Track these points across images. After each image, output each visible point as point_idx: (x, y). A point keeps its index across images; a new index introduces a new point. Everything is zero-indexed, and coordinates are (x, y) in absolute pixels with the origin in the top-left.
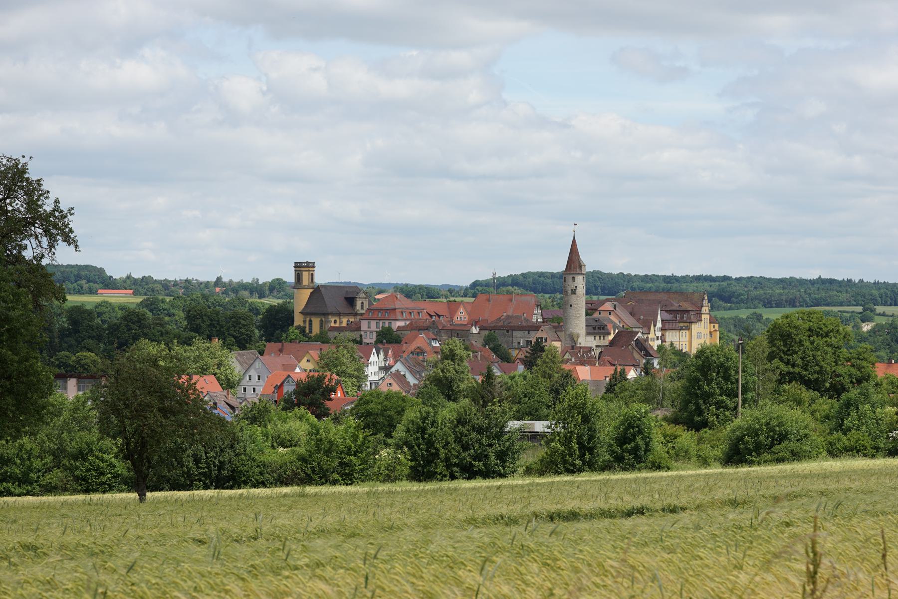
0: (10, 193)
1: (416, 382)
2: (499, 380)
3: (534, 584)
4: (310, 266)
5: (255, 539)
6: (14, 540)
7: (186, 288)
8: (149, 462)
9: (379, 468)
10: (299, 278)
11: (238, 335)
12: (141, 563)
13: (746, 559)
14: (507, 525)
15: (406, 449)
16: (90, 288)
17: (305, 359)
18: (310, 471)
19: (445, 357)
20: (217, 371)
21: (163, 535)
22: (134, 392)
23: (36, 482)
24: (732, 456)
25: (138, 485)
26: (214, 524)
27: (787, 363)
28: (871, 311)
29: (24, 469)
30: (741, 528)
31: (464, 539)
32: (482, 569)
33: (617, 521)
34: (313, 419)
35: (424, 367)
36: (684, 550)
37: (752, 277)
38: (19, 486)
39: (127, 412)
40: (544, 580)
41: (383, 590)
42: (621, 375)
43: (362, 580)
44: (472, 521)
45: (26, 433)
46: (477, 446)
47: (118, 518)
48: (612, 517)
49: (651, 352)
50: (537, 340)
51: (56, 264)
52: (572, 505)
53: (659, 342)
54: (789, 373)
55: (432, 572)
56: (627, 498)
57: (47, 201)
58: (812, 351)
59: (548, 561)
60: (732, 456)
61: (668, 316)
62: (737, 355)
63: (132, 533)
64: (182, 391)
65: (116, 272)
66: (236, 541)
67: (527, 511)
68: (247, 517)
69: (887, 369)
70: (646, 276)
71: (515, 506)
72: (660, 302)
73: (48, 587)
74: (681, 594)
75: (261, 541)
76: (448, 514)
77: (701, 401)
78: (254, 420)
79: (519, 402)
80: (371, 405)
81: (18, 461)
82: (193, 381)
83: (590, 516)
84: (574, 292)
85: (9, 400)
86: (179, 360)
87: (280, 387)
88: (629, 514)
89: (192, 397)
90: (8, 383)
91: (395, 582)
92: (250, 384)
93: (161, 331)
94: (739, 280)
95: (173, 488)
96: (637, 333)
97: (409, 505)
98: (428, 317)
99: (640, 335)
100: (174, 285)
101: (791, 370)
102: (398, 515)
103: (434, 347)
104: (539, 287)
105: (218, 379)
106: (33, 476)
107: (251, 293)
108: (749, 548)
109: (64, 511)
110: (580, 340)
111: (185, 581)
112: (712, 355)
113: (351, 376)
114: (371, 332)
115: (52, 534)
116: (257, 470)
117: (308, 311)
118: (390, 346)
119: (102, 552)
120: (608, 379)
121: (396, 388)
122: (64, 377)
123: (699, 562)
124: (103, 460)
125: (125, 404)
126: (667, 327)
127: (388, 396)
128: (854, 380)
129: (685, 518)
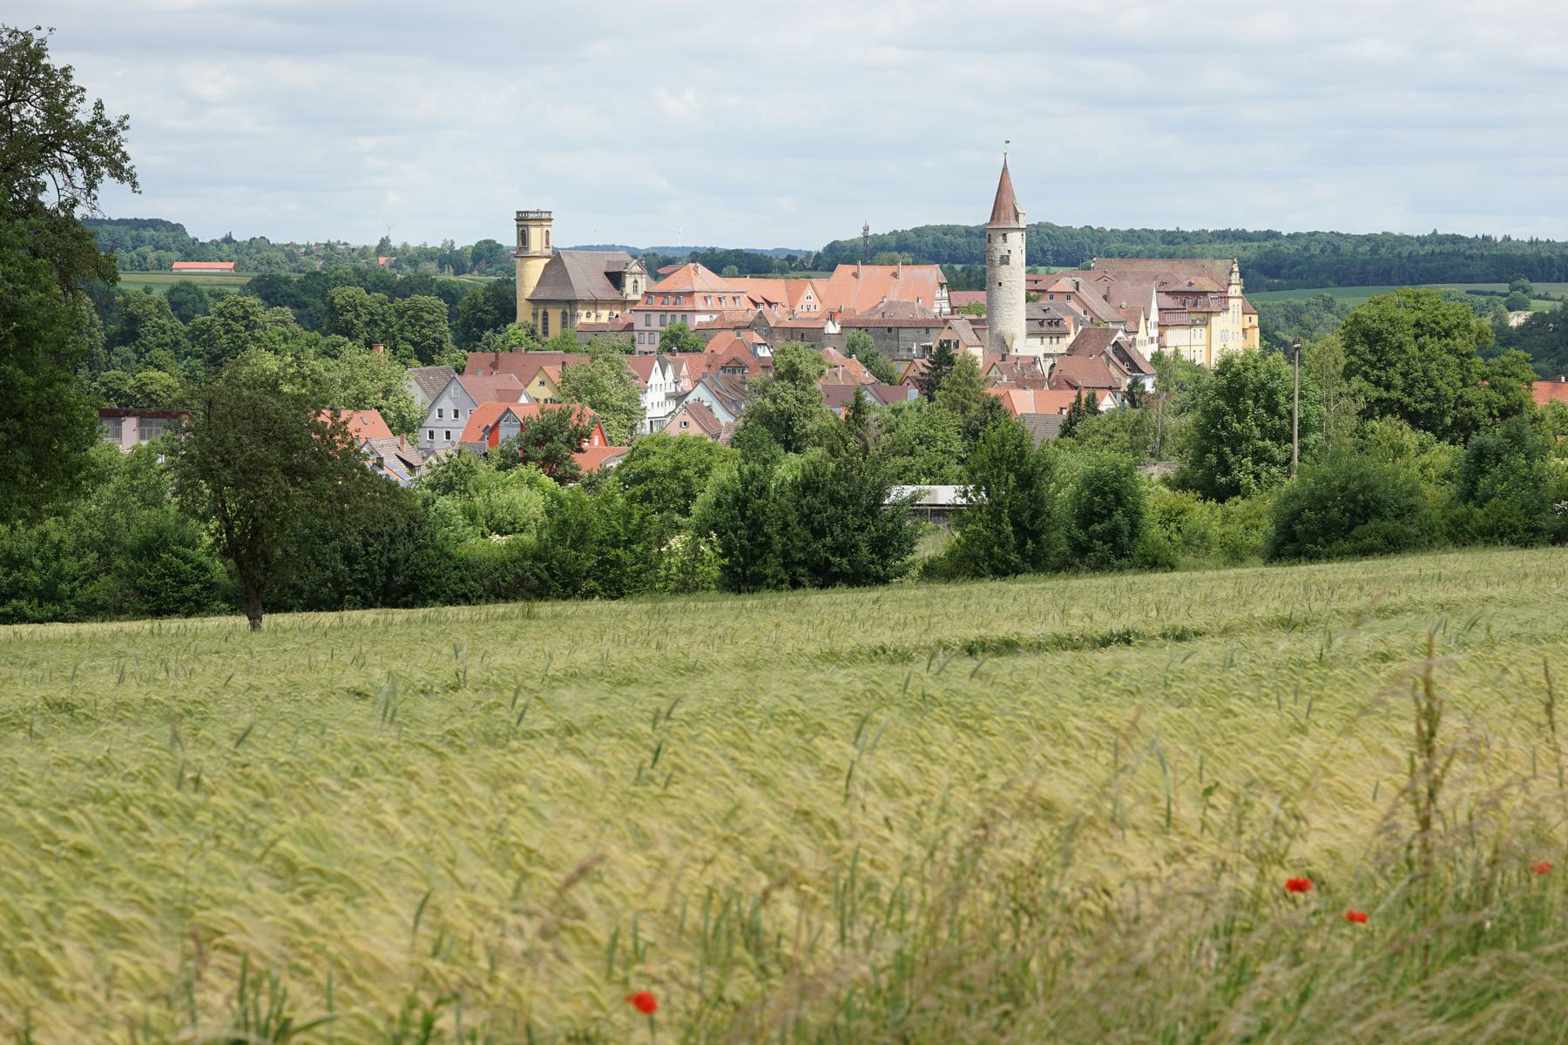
0: (16, 91)
1: (731, 420)
2: (874, 415)
3: (945, 760)
4: (542, 219)
5: (455, 688)
6: (35, 695)
7: (328, 259)
8: (267, 561)
9: (668, 569)
10: (523, 238)
11: (418, 339)
12: (259, 731)
13: (1314, 716)
14: (892, 662)
15: (714, 536)
16: (159, 260)
17: (537, 380)
18: (546, 575)
19: (780, 377)
20: (383, 403)
21: (294, 684)
22: (238, 439)
23: (69, 597)
24: (1283, 544)
25: (247, 600)
26: (382, 665)
27: (1377, 383)
28: (1525, 291)
29: (48, 576)
30: (1303, 664)
31: (819, 685)
32: (858, 734)
33: (1088, 655)
34: (549, 482)
35: (743, 393)
36: (1203, 701)
37: (1316, 233)
38: (40, 605)
39: (227, 474)
40: (962, 753)
41: (683, 771)
42: (1088, 404)
43: (649, 756)
44: (831, 657)
45: (50, 512)
46: (837, 530)
47: (215, 658)
48: (1075, 648)
49: (1140, 365)
50: (941, 344)
51: (99, 217)
52: (1005, 628)
53: (1154, 348)
54: (1379, 400)
55: (769, 740)
56: (1100, 616)
57: (81, 106)
58: (1422, 361)
59: (969, 722)
60: (1283, 544)
61: (1170, 302)
62: (1290, 367)
63: (240, 680)
64: (323, 437)
65: (203, 230)
66: (422, 692)
67: (930, 639)
68: (439, 653)
69: (1551, 392)
70: (1132, 231)
71: (906, 632)
72: (1155, 278)
73: (98, 771)
74: (1201, 776)
75: (465, 696)
76: (789, 645)
77: (1227, 450)
78: (449, 488)
79: (911, 454)
80: (653, 459)
81: (37, 562)
82: (342, 419)
83: (1038, 647)
84: (1005, 260)
85: (21, 454)
86: (316, 382)
87: (492, 431)
88: (1105, 642)
89: (340, 447)
90: (17, 425)
91: (703, 758)
92: (440, 424)
93: (283, 334)
94: (1293, 237)
95: (308, 608)
96: (1116, 331)
97: (720, 631)
98: (751, 306)
99: (1120, 334)
100: (306, 254)
101: (1385, 395)
102: (702, 647)
103: (761, 359)
104: (945, 253)
105: (384, 416)
106: (65, 587)
107: (441, 266)
108: (1319, 698)
109: (118, 646)
110: (1016, 345)
111: (338, 760)
112: (1246, 370)
113: (617, 410)
114: (651, 332)
115: (102, 685)
116: (455, 575)
117: (541, 296)
118: (684, 356)
119: (189, 713)
120: (1065, 412)
121: (694, 430)
122: (116, 416)
123: (1232, 721)
124: (185, 559)
125: (223, 460)
126: (1169, 319)
127: (682, 445)
128: (1495, 412)
129: (1206, 650)
